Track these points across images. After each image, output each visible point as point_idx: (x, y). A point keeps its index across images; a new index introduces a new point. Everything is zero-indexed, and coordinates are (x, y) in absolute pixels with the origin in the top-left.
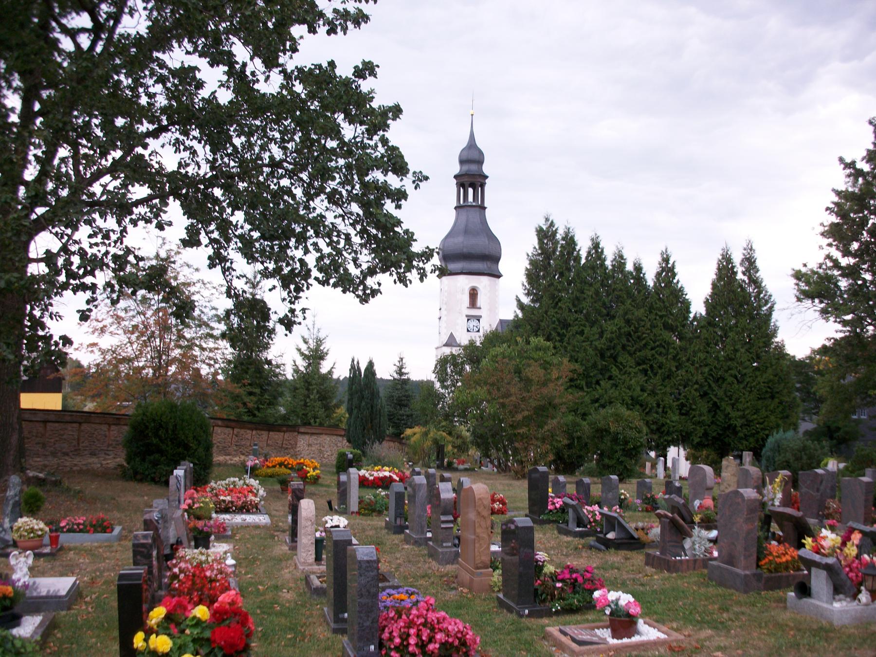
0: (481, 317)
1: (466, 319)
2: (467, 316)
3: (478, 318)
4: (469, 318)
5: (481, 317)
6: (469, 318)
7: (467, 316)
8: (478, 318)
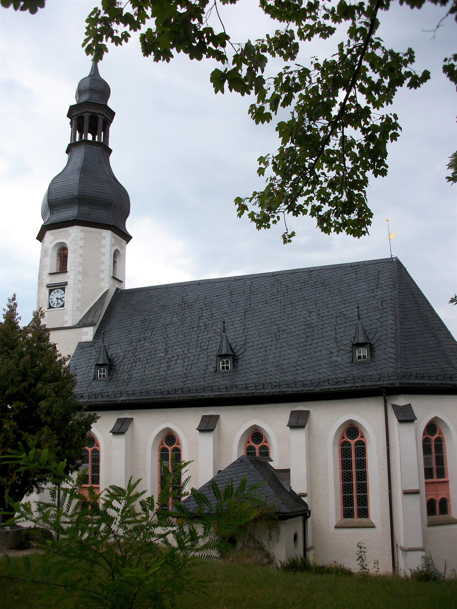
0: (66, 284)
1: (47, 291)
2: (48, 286)
3: (62, 286)
4: (52, 288)
5: (66, 284)
6: (52, 288)
7: (48, 286)
8: (62, 286)
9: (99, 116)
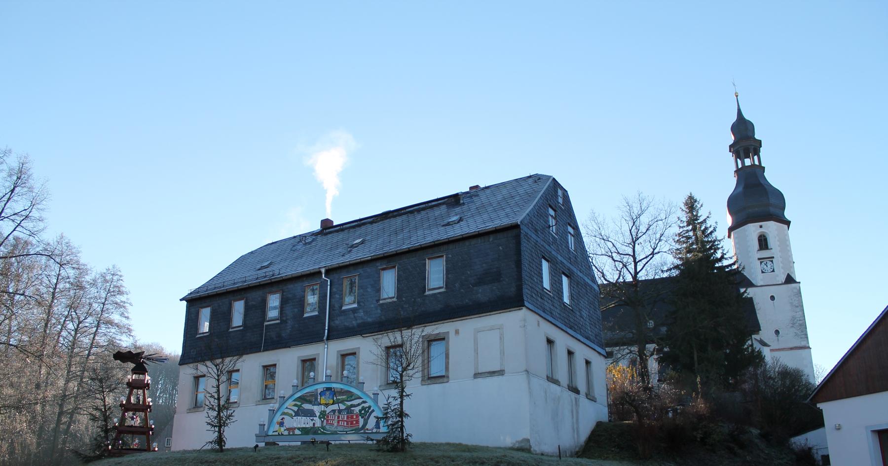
9: (749, 147)
